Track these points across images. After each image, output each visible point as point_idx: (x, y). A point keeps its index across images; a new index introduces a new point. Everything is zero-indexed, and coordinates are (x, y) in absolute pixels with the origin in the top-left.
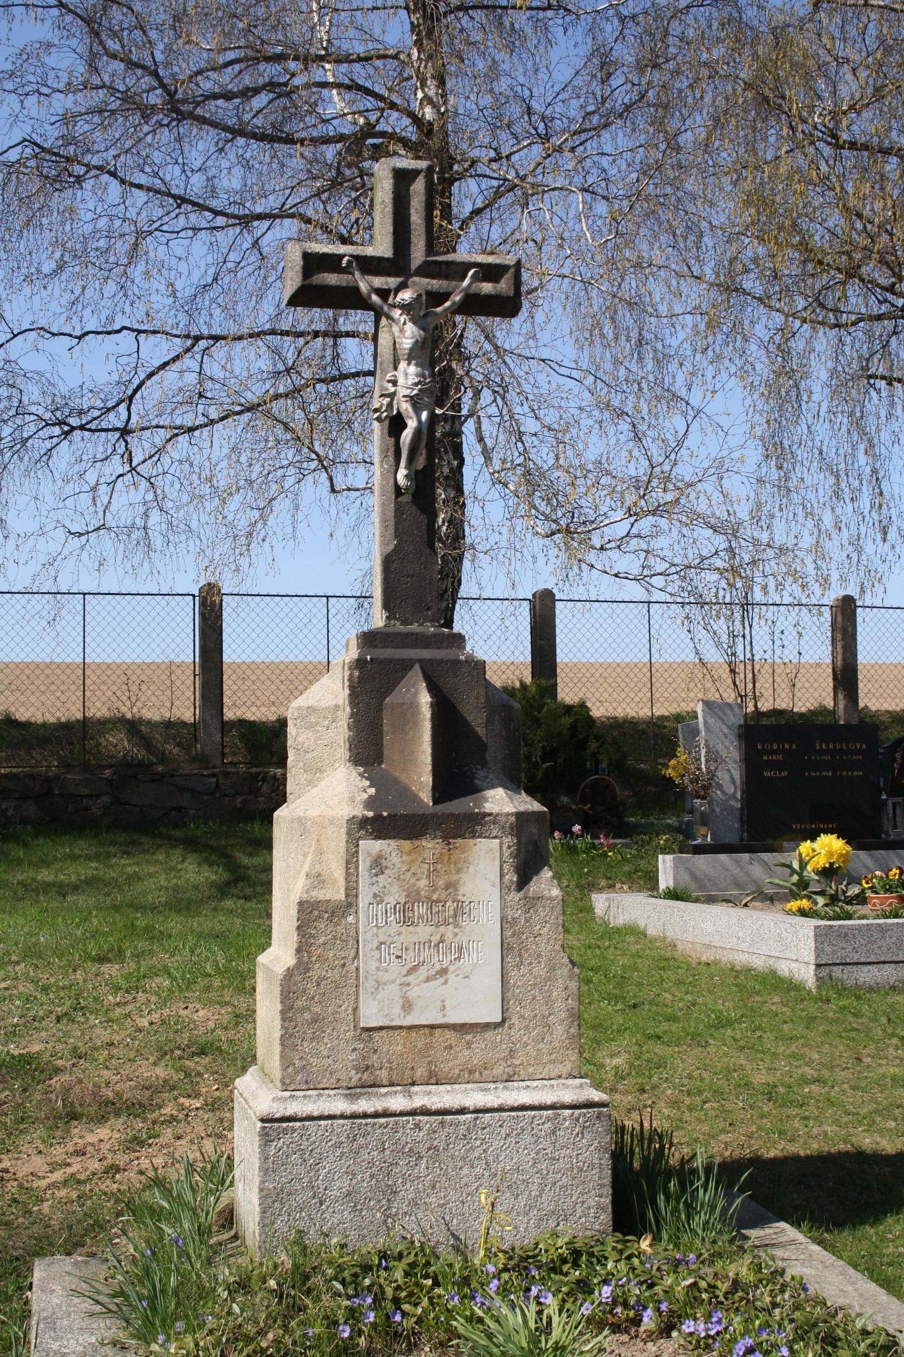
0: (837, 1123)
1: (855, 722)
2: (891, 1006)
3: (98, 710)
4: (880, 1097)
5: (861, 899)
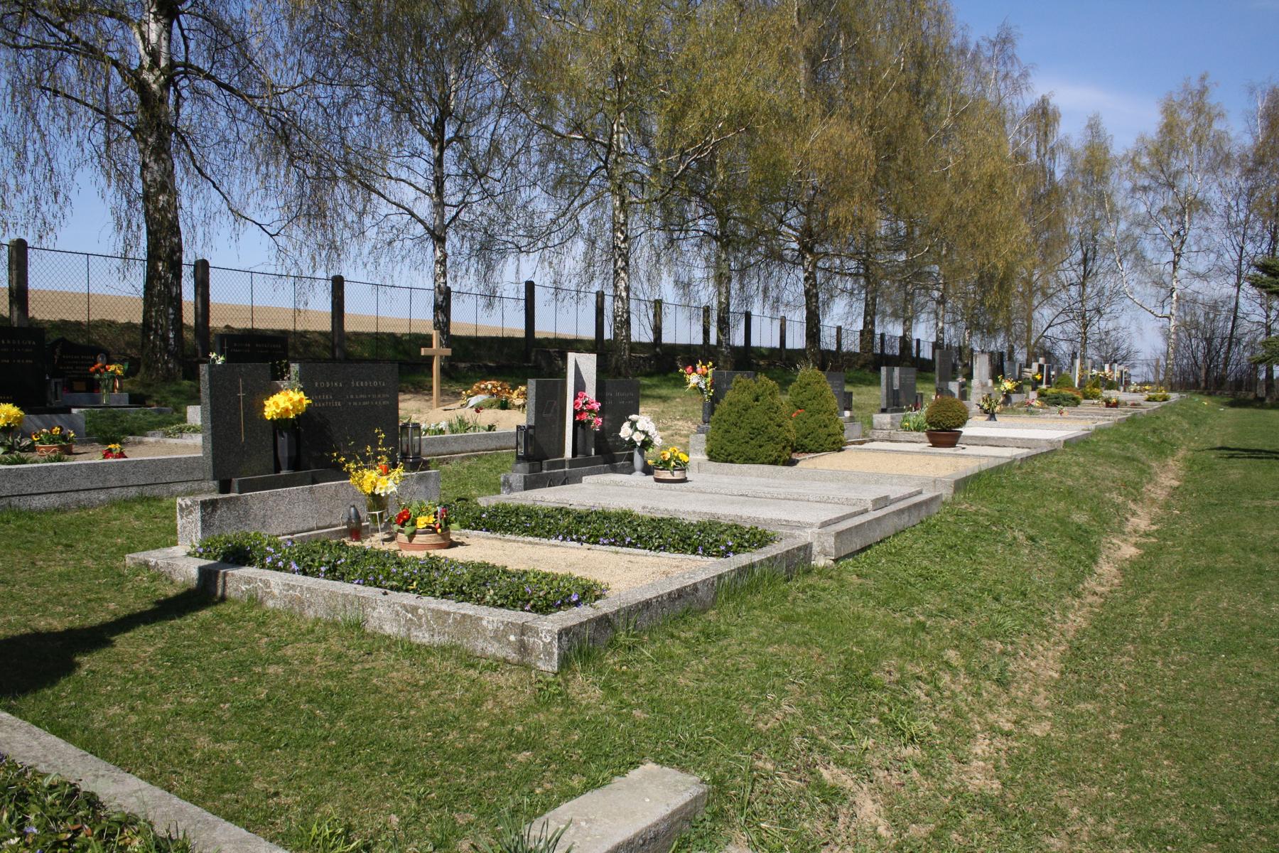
0: (18, 612)
1: (26, 325)
2: (57, 523)
3: (95, 317)
4: (51, 589)
5: (31, 448)
